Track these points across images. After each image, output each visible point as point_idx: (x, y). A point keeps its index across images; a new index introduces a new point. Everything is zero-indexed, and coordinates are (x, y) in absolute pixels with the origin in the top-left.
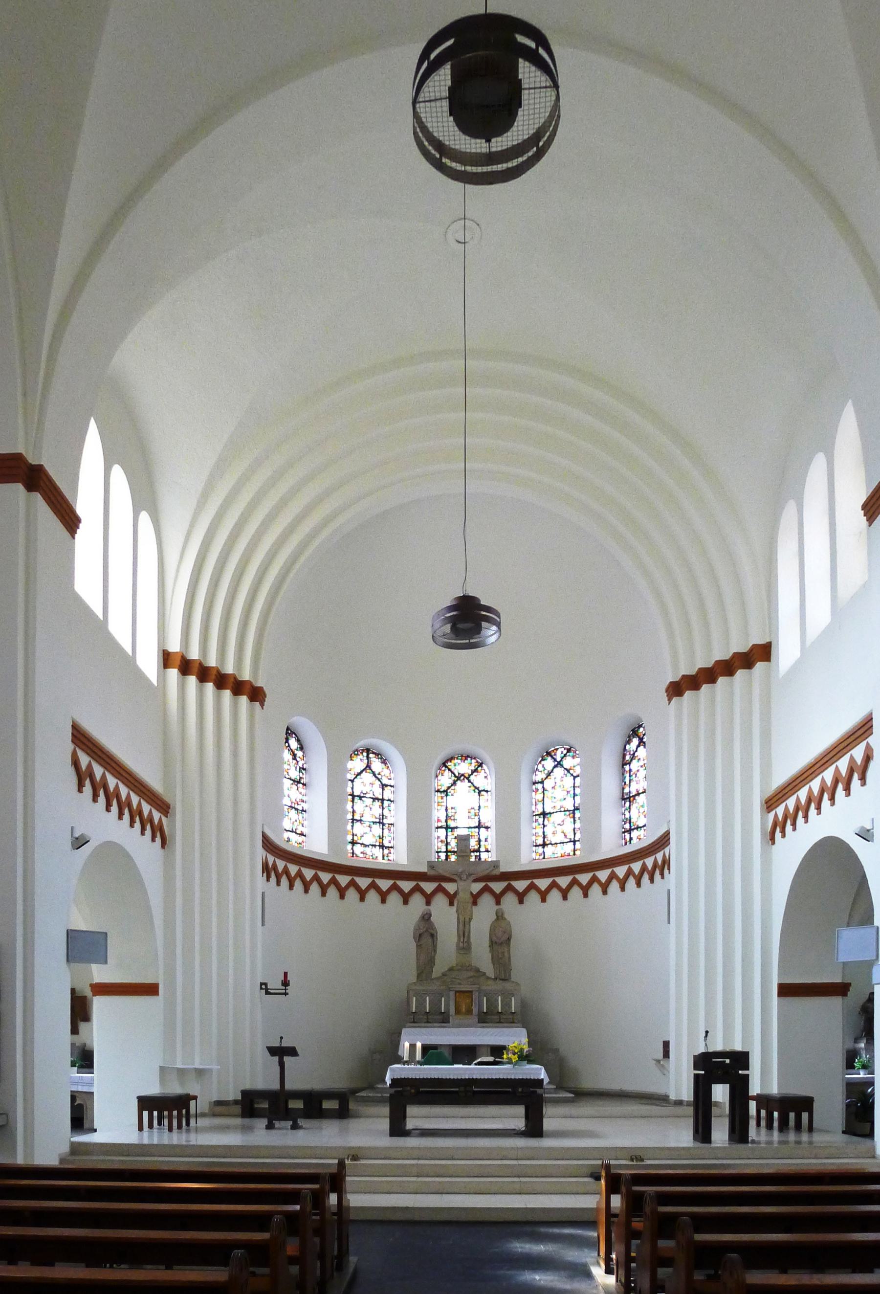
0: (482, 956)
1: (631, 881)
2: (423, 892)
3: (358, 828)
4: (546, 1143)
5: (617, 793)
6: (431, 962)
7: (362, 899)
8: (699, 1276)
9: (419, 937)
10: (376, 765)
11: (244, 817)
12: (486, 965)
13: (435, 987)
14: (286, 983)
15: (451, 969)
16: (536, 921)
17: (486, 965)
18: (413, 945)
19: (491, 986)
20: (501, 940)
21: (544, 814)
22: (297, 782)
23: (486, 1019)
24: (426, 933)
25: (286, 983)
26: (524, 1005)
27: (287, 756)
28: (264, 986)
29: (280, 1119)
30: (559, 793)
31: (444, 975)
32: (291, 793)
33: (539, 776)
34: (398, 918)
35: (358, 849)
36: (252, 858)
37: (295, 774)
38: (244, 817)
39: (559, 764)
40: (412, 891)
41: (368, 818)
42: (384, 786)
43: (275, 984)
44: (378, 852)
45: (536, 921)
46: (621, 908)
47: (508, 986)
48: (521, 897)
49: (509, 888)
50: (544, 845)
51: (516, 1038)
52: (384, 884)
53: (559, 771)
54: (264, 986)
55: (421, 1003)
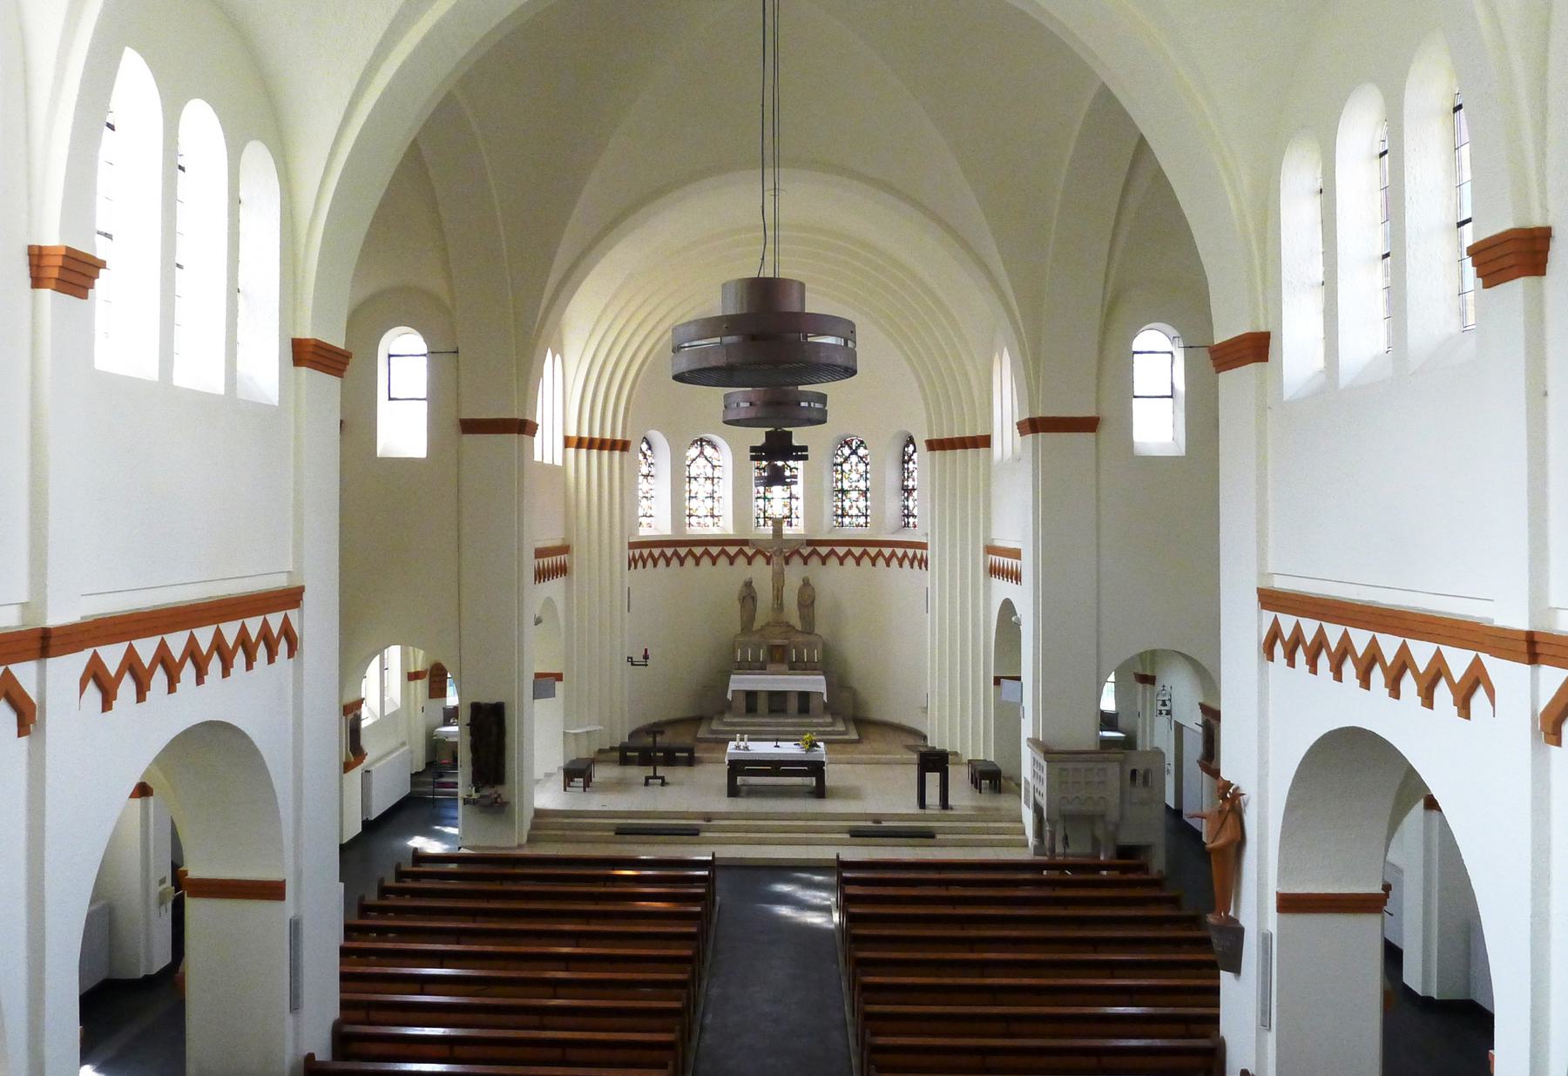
0: (793, 615)
1: (906, 563)
2: (745, 554)
3: (694, 504)
4: (829, 806)
5: (898, 485)
6: (752, 618)
7: (697, 564)
8: (819, 911)
9: (743, 600)
10: (708, 450)
11: (617, 532)
12: (795, 621)
13: (756, 638)
14: (646, 657)
15: (768, 624)
16: (835, 580)
17: (795, 621)
18: (737, 605)
19: (800, 639)
20: (807, 602)
21: (843, 491)
22: (646, 476)
23: (798, 666)
24: (748, 595)
25: (646, 657)
26: (827, 651)
27: (641, 457)
28: (630, 660)
29: (93, 218)
30: (855, 476)
31: (762, 628)
32: (643, 485)
33: (840, 460)
34: (726, 578)
35: (694, 520)
36: (622, 557)
37: (645, 470)
38: (617, 532)
39: (854, 452)
40: (737, 555)
41: (701, 496)
42: (714, 467)
43: (638, 657)
44: (709, 520)
45: (835, 580)
46: (901, 578)
47: (811, 638)
48: (824, 560)
49: (814, 552)
50: (843, 516)
51: (815, 684)
52: (715, 550)
53: (854, 459)
54: (630, 660)
55: (744, 653)
